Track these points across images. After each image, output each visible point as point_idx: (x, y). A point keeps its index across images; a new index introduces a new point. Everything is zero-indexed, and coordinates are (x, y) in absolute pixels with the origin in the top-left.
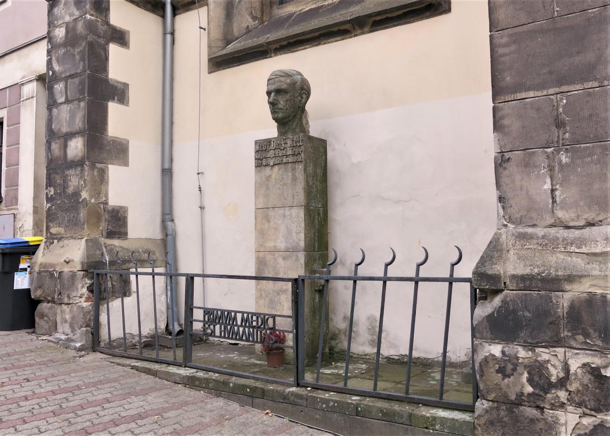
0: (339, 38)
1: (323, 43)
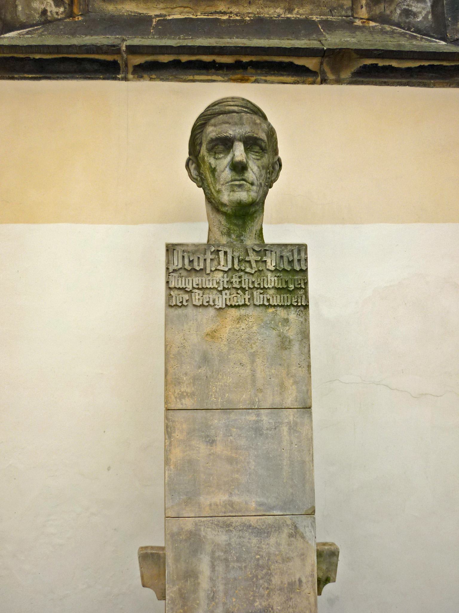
0: (290, 79)
1: (253, 79)
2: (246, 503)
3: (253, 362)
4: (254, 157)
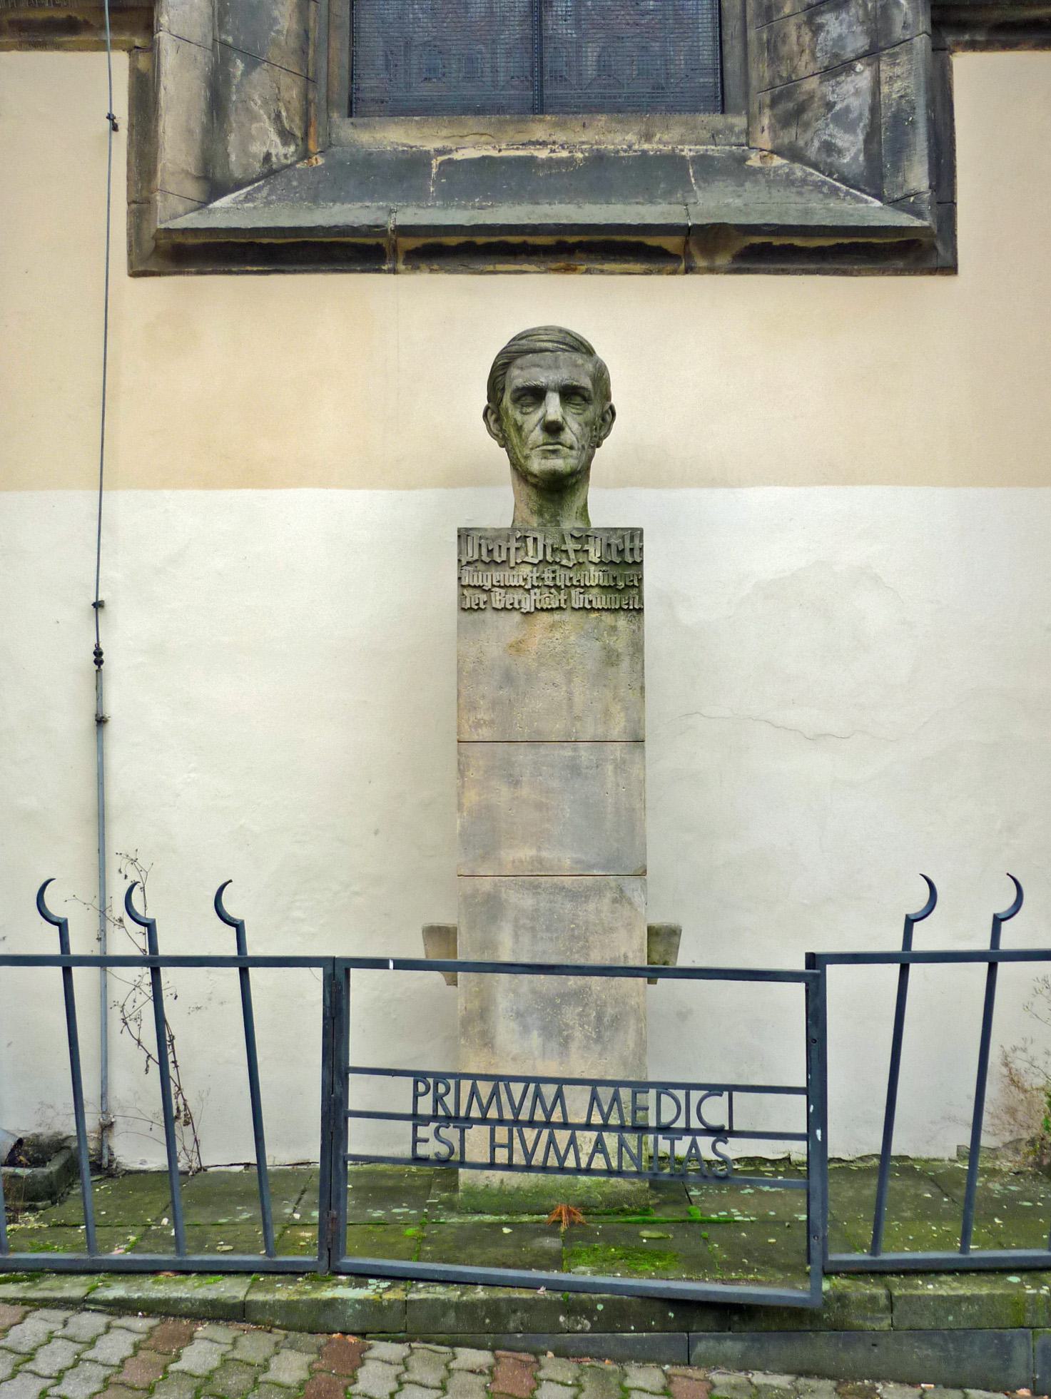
1: (584, 268)
2: (559, 860)
3: (570, 681)
4: (573, 411)
